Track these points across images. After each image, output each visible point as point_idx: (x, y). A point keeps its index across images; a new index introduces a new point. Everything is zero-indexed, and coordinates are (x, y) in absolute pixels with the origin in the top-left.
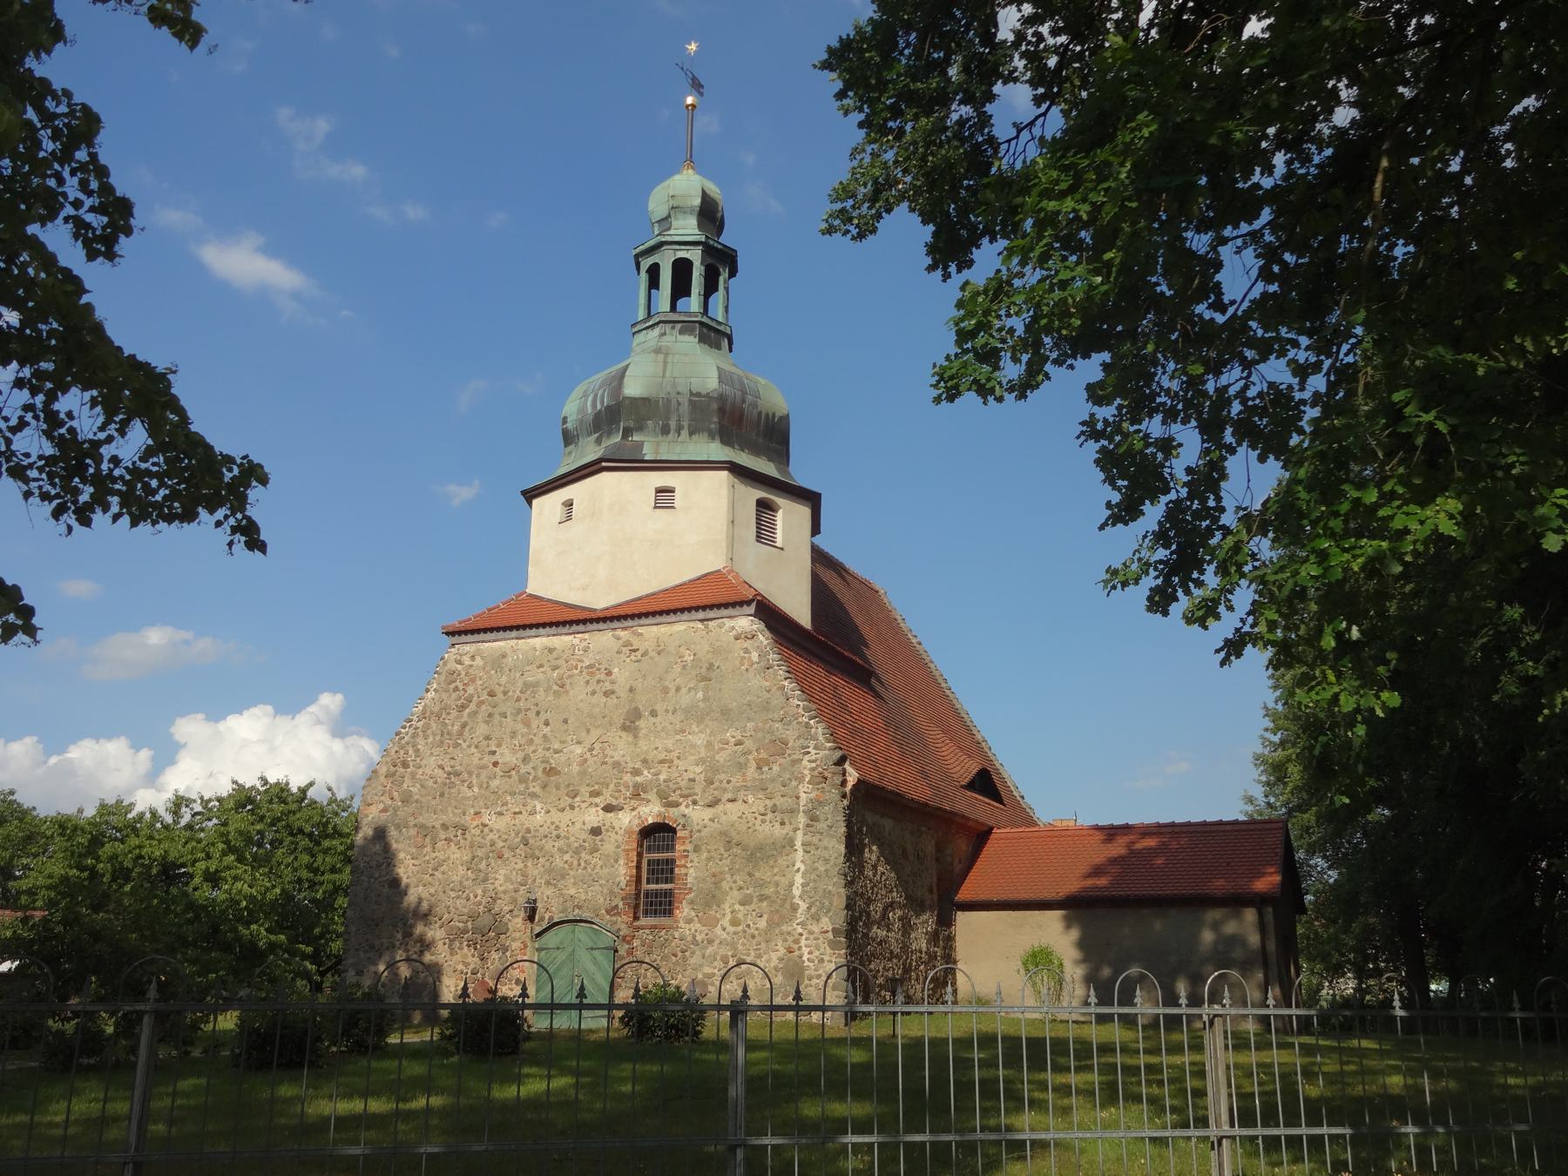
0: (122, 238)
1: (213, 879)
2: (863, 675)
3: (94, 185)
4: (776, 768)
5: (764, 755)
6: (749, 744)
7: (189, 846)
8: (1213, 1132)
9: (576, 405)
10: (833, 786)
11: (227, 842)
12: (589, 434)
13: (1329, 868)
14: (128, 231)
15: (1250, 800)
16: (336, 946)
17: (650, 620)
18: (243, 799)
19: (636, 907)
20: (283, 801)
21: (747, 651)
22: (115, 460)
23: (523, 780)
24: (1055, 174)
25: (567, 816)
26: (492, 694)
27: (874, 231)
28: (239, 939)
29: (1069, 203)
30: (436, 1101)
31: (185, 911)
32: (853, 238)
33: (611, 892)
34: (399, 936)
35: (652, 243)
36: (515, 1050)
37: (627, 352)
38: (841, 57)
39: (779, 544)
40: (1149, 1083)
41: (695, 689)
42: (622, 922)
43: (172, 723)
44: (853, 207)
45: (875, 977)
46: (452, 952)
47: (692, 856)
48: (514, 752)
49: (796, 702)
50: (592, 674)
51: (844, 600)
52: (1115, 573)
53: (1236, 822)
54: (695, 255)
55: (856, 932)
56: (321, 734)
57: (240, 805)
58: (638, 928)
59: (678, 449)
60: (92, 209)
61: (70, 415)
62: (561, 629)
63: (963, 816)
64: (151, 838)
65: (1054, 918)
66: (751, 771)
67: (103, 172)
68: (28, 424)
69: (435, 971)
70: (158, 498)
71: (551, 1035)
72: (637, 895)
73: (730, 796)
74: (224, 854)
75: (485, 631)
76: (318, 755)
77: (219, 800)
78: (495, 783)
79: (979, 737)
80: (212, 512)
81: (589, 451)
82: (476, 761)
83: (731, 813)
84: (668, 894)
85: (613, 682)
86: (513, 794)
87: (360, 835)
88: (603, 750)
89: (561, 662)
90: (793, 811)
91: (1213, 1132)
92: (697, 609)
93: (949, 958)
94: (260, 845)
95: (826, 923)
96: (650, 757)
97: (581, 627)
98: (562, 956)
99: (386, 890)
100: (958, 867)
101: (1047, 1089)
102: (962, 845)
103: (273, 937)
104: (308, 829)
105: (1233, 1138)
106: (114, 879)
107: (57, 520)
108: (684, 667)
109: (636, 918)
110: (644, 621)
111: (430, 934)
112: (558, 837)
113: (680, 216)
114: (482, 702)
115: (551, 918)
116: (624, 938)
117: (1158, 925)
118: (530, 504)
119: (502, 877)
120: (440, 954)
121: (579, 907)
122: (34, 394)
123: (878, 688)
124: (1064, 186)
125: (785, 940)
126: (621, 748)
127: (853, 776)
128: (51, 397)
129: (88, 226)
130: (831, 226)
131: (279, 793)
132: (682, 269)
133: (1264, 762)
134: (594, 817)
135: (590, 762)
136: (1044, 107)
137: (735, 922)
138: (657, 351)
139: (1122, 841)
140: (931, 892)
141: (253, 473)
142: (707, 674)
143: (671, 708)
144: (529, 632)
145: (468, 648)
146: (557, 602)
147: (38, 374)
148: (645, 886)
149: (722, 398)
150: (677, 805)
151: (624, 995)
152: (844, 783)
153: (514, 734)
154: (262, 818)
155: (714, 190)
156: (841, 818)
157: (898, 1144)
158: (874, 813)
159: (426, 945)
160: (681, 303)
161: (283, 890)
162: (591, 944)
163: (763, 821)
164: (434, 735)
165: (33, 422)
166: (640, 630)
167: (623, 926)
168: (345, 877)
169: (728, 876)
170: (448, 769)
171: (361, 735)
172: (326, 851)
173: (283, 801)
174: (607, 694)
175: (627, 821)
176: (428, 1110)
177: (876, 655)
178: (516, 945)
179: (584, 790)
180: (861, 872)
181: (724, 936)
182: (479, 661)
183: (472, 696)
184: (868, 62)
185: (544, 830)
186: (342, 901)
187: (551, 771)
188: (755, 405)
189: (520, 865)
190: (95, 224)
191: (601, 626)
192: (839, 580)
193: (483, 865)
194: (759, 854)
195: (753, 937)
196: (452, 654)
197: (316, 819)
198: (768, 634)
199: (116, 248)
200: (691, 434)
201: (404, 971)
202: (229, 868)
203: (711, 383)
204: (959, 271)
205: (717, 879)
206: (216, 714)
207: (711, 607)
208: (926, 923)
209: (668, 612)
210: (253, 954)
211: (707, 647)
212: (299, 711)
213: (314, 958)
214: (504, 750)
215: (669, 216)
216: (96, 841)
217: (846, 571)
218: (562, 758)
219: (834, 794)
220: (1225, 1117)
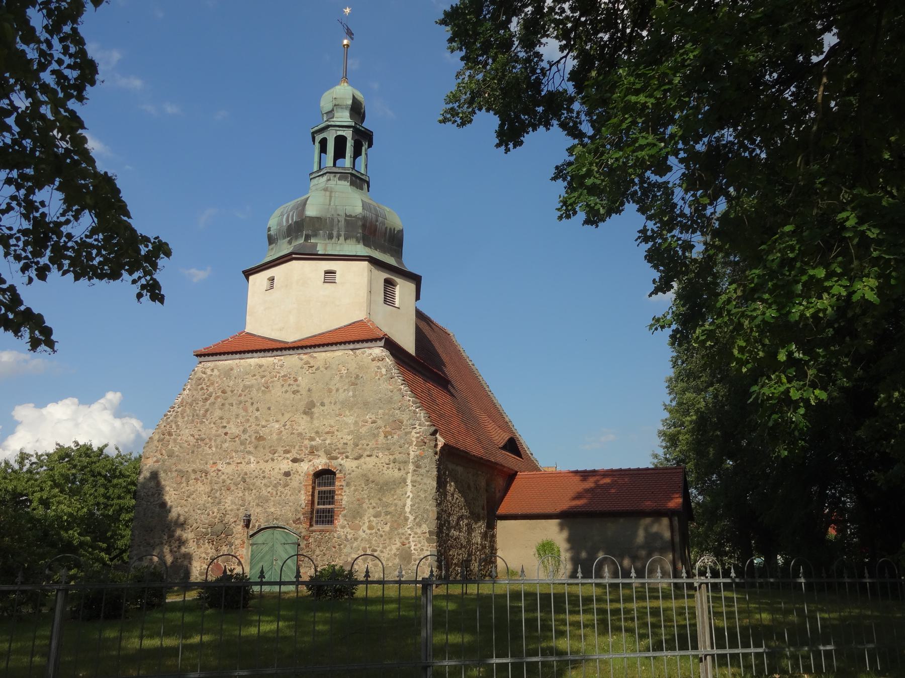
0: (88, 87)
1: (45, 503)
2: (443, 383)
3: (72, 50)
4: (396, 437)
5: (388, 429)
7: (30, 483)
8: (701, 652)
9: (276, 221)
10: (430, 447)
11: (54, 481)
12: (284, 238)
13: (699, 494)
14: (93, 83)
15: (656, 456)
17: (321, 349)
18: (63, 454)
19: (311, 518)
21: (379, 368)
22: (70, 236)
23: (242, 443)
24: (632, 79)
26: (224, 392)
27: (470, 121)
29: (642, 98)
30: (206, 638)
32: (458, 126)
33: (296, 510)
34: (166, 537)
36: (245, 606)
37: (307, 190)
38: (452, 17)
40: (626, 619)
41: (348, 390)
42: (303, 528)
44: (459, 107)
45: (452, 559)
46: (199, 547)
47: (345, 488)
48: (237, 426)
49: (408, 398)
51: (431, 339)
52: (658, 320)
53: (647, 469)
54: (348, 134)
55: (442, 533)
56: (107, 416)
57: (62, 458)
58: (313, 532)
59: (338, 248)
60: (69, 66)
61: (42, 204)
62: (267, 354)
63: (502, 465)
65: (553, 524)
66: (381, 438)
67: (79, 41)
68: (13, 209)
69: (188, 557)
70: (95, 263)
71: (262, 596)
72: (312, 512)
73: (368, 453)
74: (52, 488)
75: (220, 354)
76: (105, 428)
77: (48, 455)
78: (226, 445)
79: (507, 419)
80: (131, 274)
81: (285, 248)
82: (214, 432)
83: (369, 463)
84: (331, 511)
85: (298, 386)
86: (236, 452)
88: (292, 425)
89: (266, 373)
90: (406, 462)
91: (701, 652)
92: (349, 342)
93: (493, 550)
95: (425, 528)
96: (320, 431)
97: (279, 353)
98: (266, 548)
99: (157, 509)
100: (498, 495)
101: (566, 624)
102: (501, 482)
103: (82, 538)
104: (104, 473)
105: (713, 656)
107: (24, 273)
109: (311, 525)
110: (317, 349)
112: (264, 477)
113: (339, 110)
114: (218, 397)
115: (259, 526)
116: (304, 537)
117: (612, 528)
118: (248, 279)
119: (229, 501)
120: (191, 548)
121: (277, 519)
122: (18, 189)
123: (452, 390)
124: (638, 86)
126: (303, 424)
127: (441, 442)
128: (30, 191)
129: (66, 78)
130: (445, 118)
131: (86, 451)
132: (340, 142)
133: (665, 434)
134: (286, 465)
136: (566, 52)
137: (370, 528)
138: (326, 190)
140: (483, 509)
141: (162, 249)
143: (333, 402)
144: (247, 355)
145: (210, 364)
147: (23, 176)
148: (316, 506)
149: (364, 218)
150: (336, 458)
151: (307, 573)
152: (436, 446)
153: (237, 416)
155: (360, 96)
156: (434, 466)
157: (522, 664)
158: (453, 463)
159: (182, 542)
160: (339, 162)
162: (283, 541)
163: (388, 468)
164: (188, 416)
165: (17, 208)
166: (315, 355)
167: (303, 530)
169: (367, 501)
171: (131, 417)
172: (115, 486)
175: (306, 467)
176: (201, 644)
177: (450, 371)
179: (280, 450)
180: (445, 498)
181: (364, 535)
182: (216, 372)
183: (212, 393)
184: (468, 21)
185: (256, 473)
187: (260, 438)
188: (384, 224)
189: (241, 494)
190: (70, 77)
191: (291, 352)
192: (428, 328)
194: (385, 487)
195: (382, 536)
196: (199, 368)
197: (109, 466)
198: (391, 358)
199: (84, 93)
201: (169, 559)
202: (55, 496)
203: (358, 210)
204: (515, 147)
205: (360, 502)
206: (41, 404)
207: (358, 342)
209: (332, 344)
210: (69, 547)
213: (108, 551)
215: (333, 110)
217: (432, 322)
218: (267, 430)
219: (430, 452)
220: (708, 643)
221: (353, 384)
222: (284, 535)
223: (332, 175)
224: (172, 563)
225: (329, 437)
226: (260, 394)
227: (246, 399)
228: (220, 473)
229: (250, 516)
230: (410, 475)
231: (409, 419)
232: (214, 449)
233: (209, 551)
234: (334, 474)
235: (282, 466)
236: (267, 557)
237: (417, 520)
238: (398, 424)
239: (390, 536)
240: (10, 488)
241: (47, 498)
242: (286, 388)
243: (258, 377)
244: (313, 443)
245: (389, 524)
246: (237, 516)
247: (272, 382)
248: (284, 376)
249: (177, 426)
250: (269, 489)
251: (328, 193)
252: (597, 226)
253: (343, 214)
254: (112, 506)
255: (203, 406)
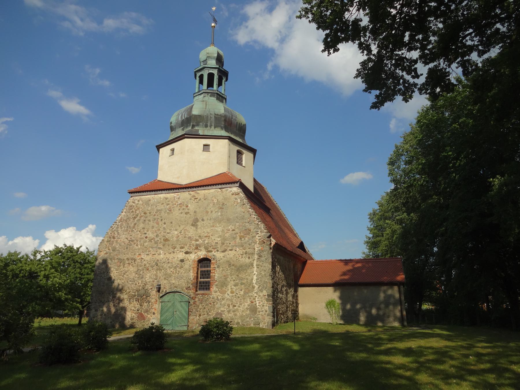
1: (47, 277)
4: (246, 239)
5: (242, 234)
6: (237, 231)
7: (39, 266)
9: (175, 118)
12: (180, 127)
15: (364, 253)
16: (88, 299)
17: (202, 188)
18: (58, 251)
19: (197, 287)
20: (71, 252)
21: (236, 199)
25: (172, 255)
26: (145, 213)
28: (55, 297)
31: (37, 288)
33: (188, 282)
34: (111, 298)
35: (201, 67)
37: (192, 102)
39: (244, 165)
41: (218, 212)
42: (191, 292)
43: (45, 233)
46: (130, 303)
47: (217, 269)
48: (153, 233)
49: (254, 216)
50: (181, 207)
54: (215, 72)
56: (89, 235)
64: (26, 264)
66: (238, 240)
69: (124, 309)
72: (197, 283)
73: (230, 248)
74: (51, 269)
75: (143, 192)
77: (50, 251)
78: (146, 244)
79: (295, 233)
81: (180, 132)
82: (139, 236)
83: (231, 254)
86: (152, 248)
87: (97, 262)
88: (185, 232)
89: (170, 202)
90: (253, 254)
92: (218, 184)
93: (297, 304)
94: (64, 266)
95: (265, 293)
96: (202, 235)
97: (177, 191)
98: (170, 304)
99: (106, 281)
102: (299, 266)
103: (66, 296)
104: (79, 261)
106: (13, 277)
108: (214, 204)
109: (196, 291)
110: (200, 188)
111: (122, 297)
112: (169, 263)
113: (210, 59)
114: (142, 216)
115: (166, 291)
116: (192, 298)
117: (365, 291)
119: (148, 277)
120: (126, 303)
125: (250, 299)
126: (191, 232)
127: (273, 242)
131: (70, 249)
132: (211, 76)
135: (180, 237)
138: (203, 101)
139: (351, 264)
142: (222, 207)
143: (209, 219)
144: (159, 192)
145: (137, 198)
146: (168, 183)
148: (199, 280)
149: (225, 116)
150: (211, 251)
152: (271, 244)
153: (153, 227)
154: (64, 257)
155: (221, 53)
156: (270, 256)
159: (120, 300)
161: (71, 281)
162: (180, 300)
163: (242, 257)
164: (124, 227)
166: (198, 192)
167: (192, 294)
168: (92, 276)
169: (230, 276)
170: (129, 239)
172: (85, 268)
173: (71, 252)
174: (186, 213)
175: (194, 257)
178: (153, 300)
179: (178, 247)
181: (228, 297)
182: (141, 202)
183: (138, 214)
185: (164, 260)
186: (91, 284)
187: (166, 240)
188: (235, 120)
189: (155, 273)
191: (184, 190)
193: (141, 273)
194: (241, 269)
195: (239, 297)
196: (131, 200)
197: (82, 258)
200: (215, 128)
201: (113, 310)
202: (52, 273)
204: (334, 52)
205: (226, 277)
206: (58, 230)
207: (223, 184)
208: (291, 291)
210: (59, 300)
211: (222, 198)
212: (83, 228)
213: (81, 303)
214: (149, 232)
215: (206, 60)
216: (7, 265)
218: (170, 235)
219: (268, 248)
221: (221, 208)
222: (180, 296)
223: (206, 94)
224: (115, 312)
225: (207, 239)
226: (166, 215)
227: (158, 217)
228: (143, 260)
229: (160, 285)
230: (255, 261)
231: (255, 228)
232: (139, 246)
233: (136, 306)
234: (210, 260)
235: (179, 256)
236: (171, 310)
237: (260, 288)
238: (248, 231)
239: (244, 297)
240: (28, 269)
241: (48, 275)
242: (181, 211)
243: (165, 204)
244: (197, 243)
245: (243, 290)
246: (153, 285)
247: (173, 207)
248: (181, 204)
249: (118, 233)
250: (172, 270)
251: (204, 103)
252: (379, 109)
253: (213, 113)
254: (84, 278)
255: (133, 221)
